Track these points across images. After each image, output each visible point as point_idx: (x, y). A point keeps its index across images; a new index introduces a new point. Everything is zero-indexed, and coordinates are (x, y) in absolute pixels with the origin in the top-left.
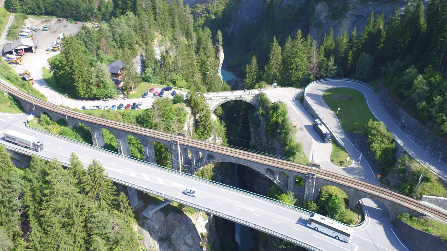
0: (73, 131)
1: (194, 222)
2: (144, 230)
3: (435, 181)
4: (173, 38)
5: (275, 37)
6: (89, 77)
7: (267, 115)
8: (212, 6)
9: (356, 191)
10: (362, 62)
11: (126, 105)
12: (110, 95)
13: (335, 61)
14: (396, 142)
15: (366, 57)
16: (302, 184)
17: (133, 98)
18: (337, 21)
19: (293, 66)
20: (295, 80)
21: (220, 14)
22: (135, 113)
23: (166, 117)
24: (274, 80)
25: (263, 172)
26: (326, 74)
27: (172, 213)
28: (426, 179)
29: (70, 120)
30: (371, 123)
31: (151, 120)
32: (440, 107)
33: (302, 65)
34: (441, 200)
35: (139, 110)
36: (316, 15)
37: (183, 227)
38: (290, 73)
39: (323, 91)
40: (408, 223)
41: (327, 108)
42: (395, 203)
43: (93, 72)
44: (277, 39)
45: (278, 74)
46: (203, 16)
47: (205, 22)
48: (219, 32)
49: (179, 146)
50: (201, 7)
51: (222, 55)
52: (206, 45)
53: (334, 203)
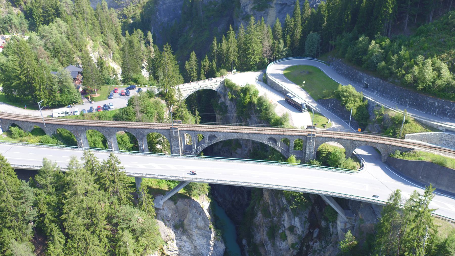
0: (54, 138)
3: (412, 122)
4: (104, 43)
5: (230, 25)
6: (52, 84)
8: (127, 10)
10: (311, 41)
12: (75, 101)
17: (99, 101)
18: (264, 12)
19: (250, 51)
20: (253, 64)
21: (138, 18)
22: (109, 113)
23: (146, 112)
24: (233, 67)
25: (265, 142)
26: (278, 56)
27: (180, 199)
28: (406, 122)
29: (48, 128)
31: (131, 117)
32: (397, 64)
33: (258, 50)
34: (421, 135)
35: (112, 111)
36: (242, 8)
37: (194, 211)
39: (282, 70)
40: (402, 158)
44: (232, 28)
45: (236, 60)
48: (149, 34)
49: (179, 132)
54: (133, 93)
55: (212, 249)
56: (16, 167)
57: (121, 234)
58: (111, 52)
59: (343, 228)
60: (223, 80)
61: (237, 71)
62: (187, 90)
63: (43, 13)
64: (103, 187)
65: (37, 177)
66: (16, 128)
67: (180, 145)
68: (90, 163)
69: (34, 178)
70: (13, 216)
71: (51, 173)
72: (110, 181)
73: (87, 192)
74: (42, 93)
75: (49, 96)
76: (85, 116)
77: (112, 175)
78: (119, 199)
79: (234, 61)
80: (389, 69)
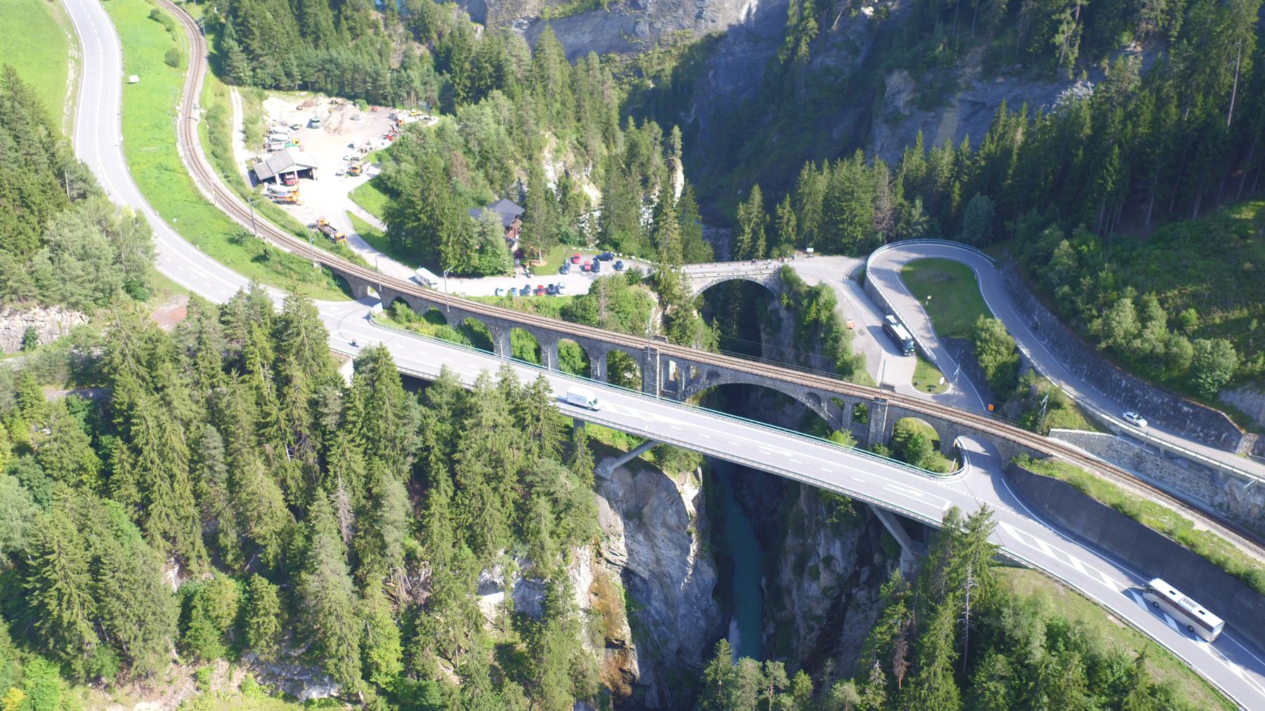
1: (679, 488)
2: (600, 497)
4: (579, 142)
7: (796, 308)
9: (951, 423)
11: (536, 288)
13: (925, 206)
14: (1021, 353)
15: (982, 202)
16: (864, 420)
18: (932, 114)
21: (667, 79)
22: (555, 302)
25: (801, 398)
27: (643, 471)
28: (1056, 405)
30: (982, 321)
38: (839, 230)
39: (900, 263)
40: (1027, 468)
41: (907, 295)
42: (1009, 440)
43: (474, 226)
46: (625, 81)
47: (629, 95)
48: (676, 131)
49: (658, 357)
50: (621, 61)
51: (679, 178)
52: (648, 159)
53: (916, 444)
54: (606, 269)
55: (690, 573)
56: (404, 371)
57: (535, 500)
58: (591, 162)
59: (908, 571)
60: (781, 265)
61: (815, 251)
62: (705, 277)
63: (471, 70)
64: (521, 424)
65: (429, 391)
66: (404, 306)
67: (658, 378)
68: (506, 383)
69: (424, 392)
70: (390, 441)
71: (450, 389)
72: (533, 416)
73: (495, 426)
74: (451, 248)
75: (461, 256)
76: (514, 300)
77: (536, 407)
78: (541, 447)
79: (811, 232)
80: (1073, 302)
